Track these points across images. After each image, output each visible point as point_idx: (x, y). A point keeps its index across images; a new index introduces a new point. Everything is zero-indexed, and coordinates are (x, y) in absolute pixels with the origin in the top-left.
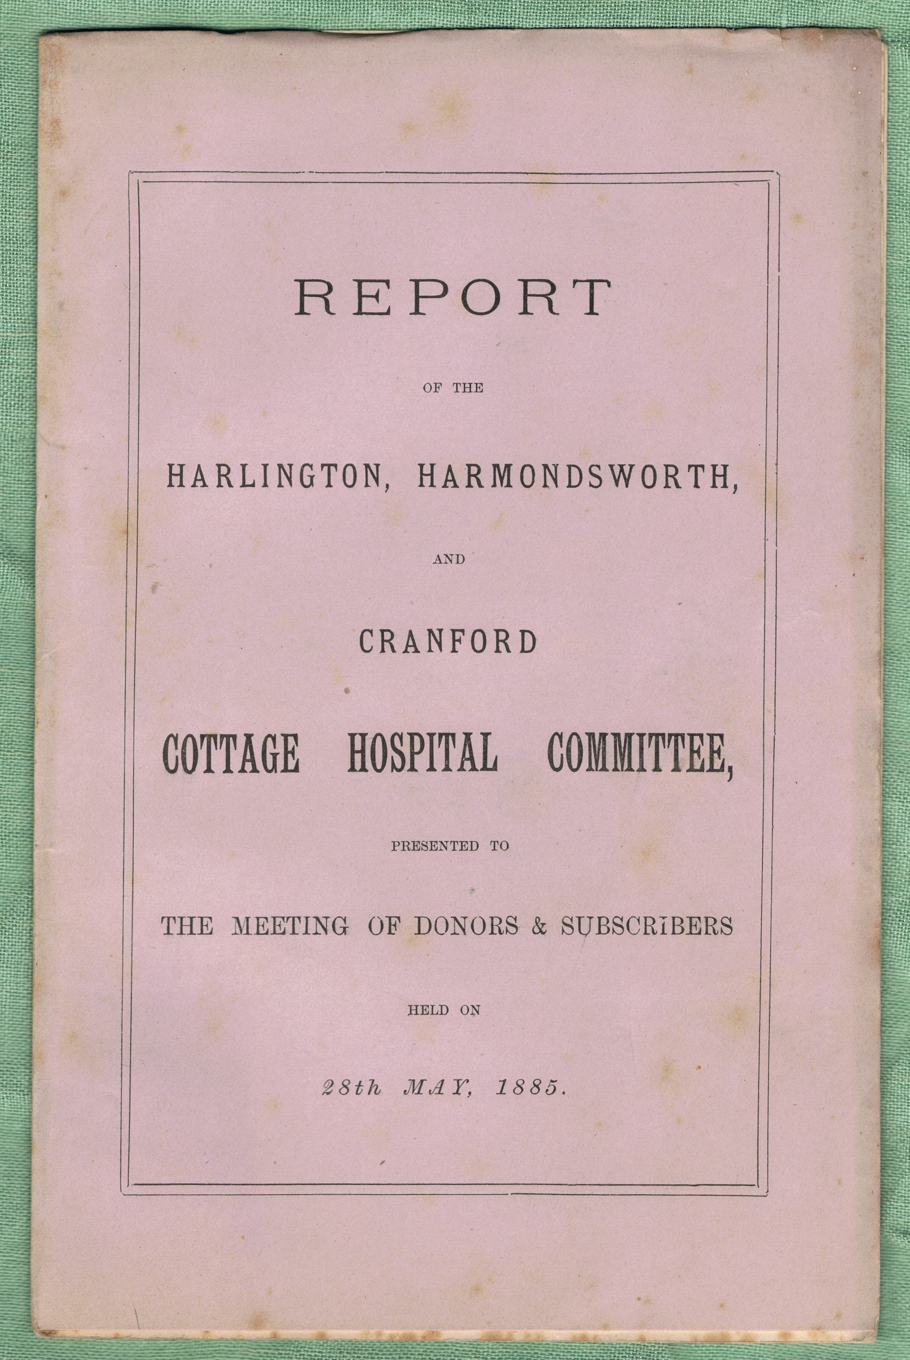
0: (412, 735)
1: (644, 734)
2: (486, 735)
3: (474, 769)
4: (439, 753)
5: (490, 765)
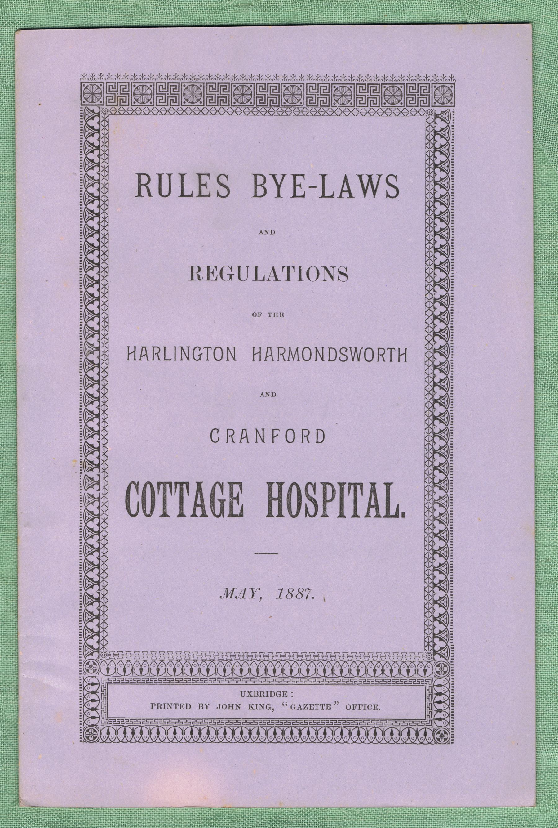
0: (325, 485)
1: (344, 484)
2: (388, 485)
3: (378, 516)
4: (349, 499)
5: (392, 512)
